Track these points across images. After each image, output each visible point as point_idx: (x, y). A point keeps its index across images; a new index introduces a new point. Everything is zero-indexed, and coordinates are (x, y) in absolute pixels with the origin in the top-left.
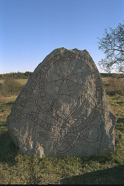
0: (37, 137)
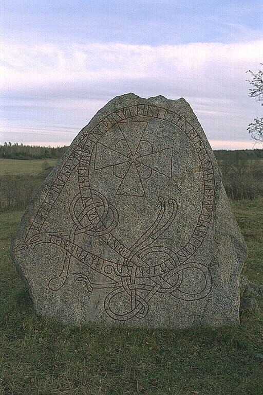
0: (70, 283)
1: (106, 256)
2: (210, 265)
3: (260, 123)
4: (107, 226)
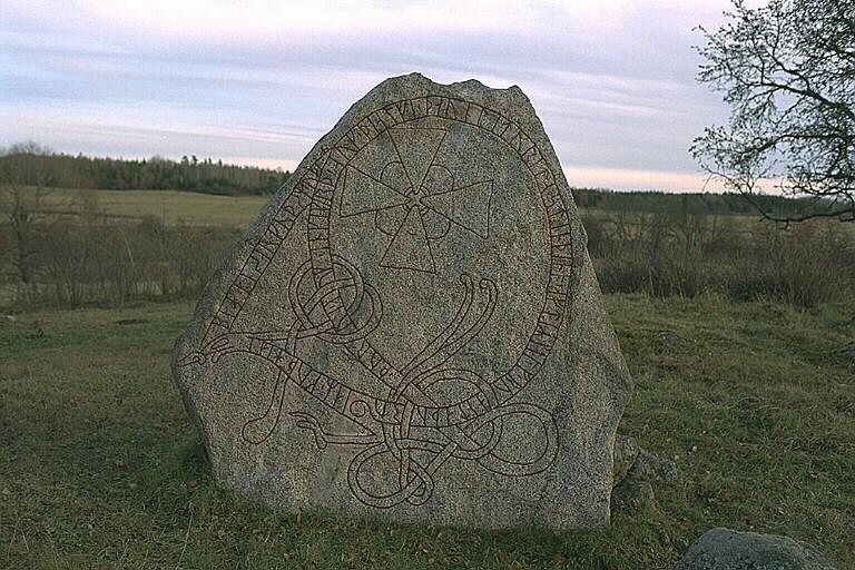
0: (283, 430)
1: (355, 381)
2: (557, 410)
3: (716, 136)
4: (359, 326)
